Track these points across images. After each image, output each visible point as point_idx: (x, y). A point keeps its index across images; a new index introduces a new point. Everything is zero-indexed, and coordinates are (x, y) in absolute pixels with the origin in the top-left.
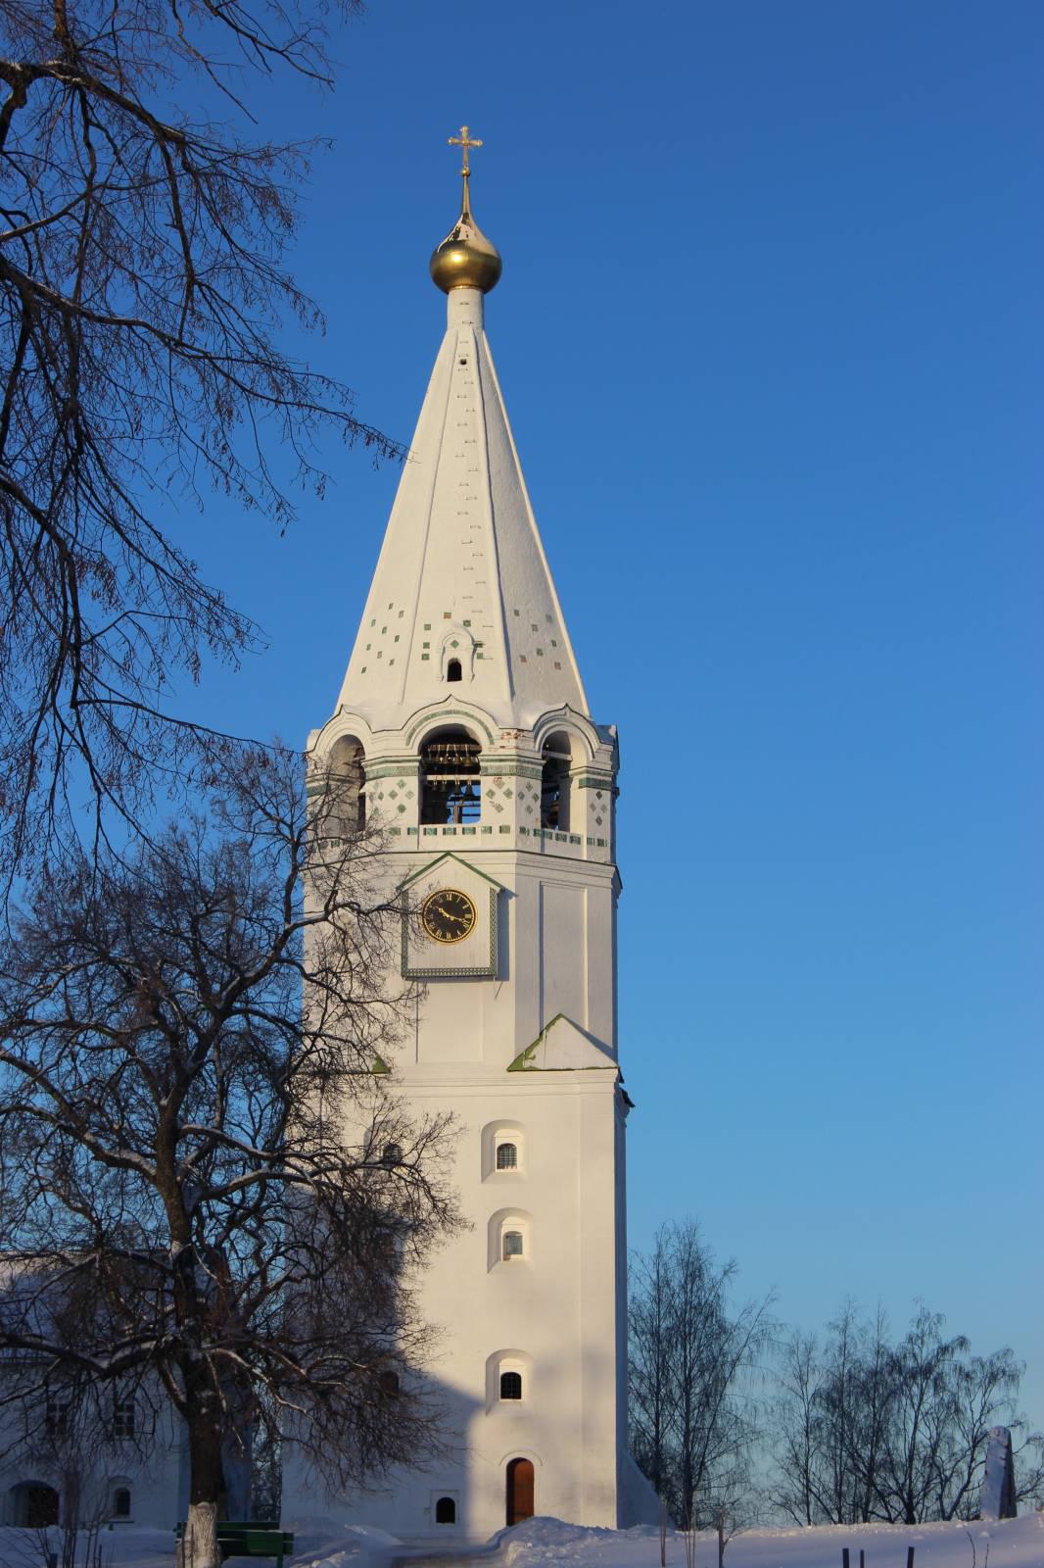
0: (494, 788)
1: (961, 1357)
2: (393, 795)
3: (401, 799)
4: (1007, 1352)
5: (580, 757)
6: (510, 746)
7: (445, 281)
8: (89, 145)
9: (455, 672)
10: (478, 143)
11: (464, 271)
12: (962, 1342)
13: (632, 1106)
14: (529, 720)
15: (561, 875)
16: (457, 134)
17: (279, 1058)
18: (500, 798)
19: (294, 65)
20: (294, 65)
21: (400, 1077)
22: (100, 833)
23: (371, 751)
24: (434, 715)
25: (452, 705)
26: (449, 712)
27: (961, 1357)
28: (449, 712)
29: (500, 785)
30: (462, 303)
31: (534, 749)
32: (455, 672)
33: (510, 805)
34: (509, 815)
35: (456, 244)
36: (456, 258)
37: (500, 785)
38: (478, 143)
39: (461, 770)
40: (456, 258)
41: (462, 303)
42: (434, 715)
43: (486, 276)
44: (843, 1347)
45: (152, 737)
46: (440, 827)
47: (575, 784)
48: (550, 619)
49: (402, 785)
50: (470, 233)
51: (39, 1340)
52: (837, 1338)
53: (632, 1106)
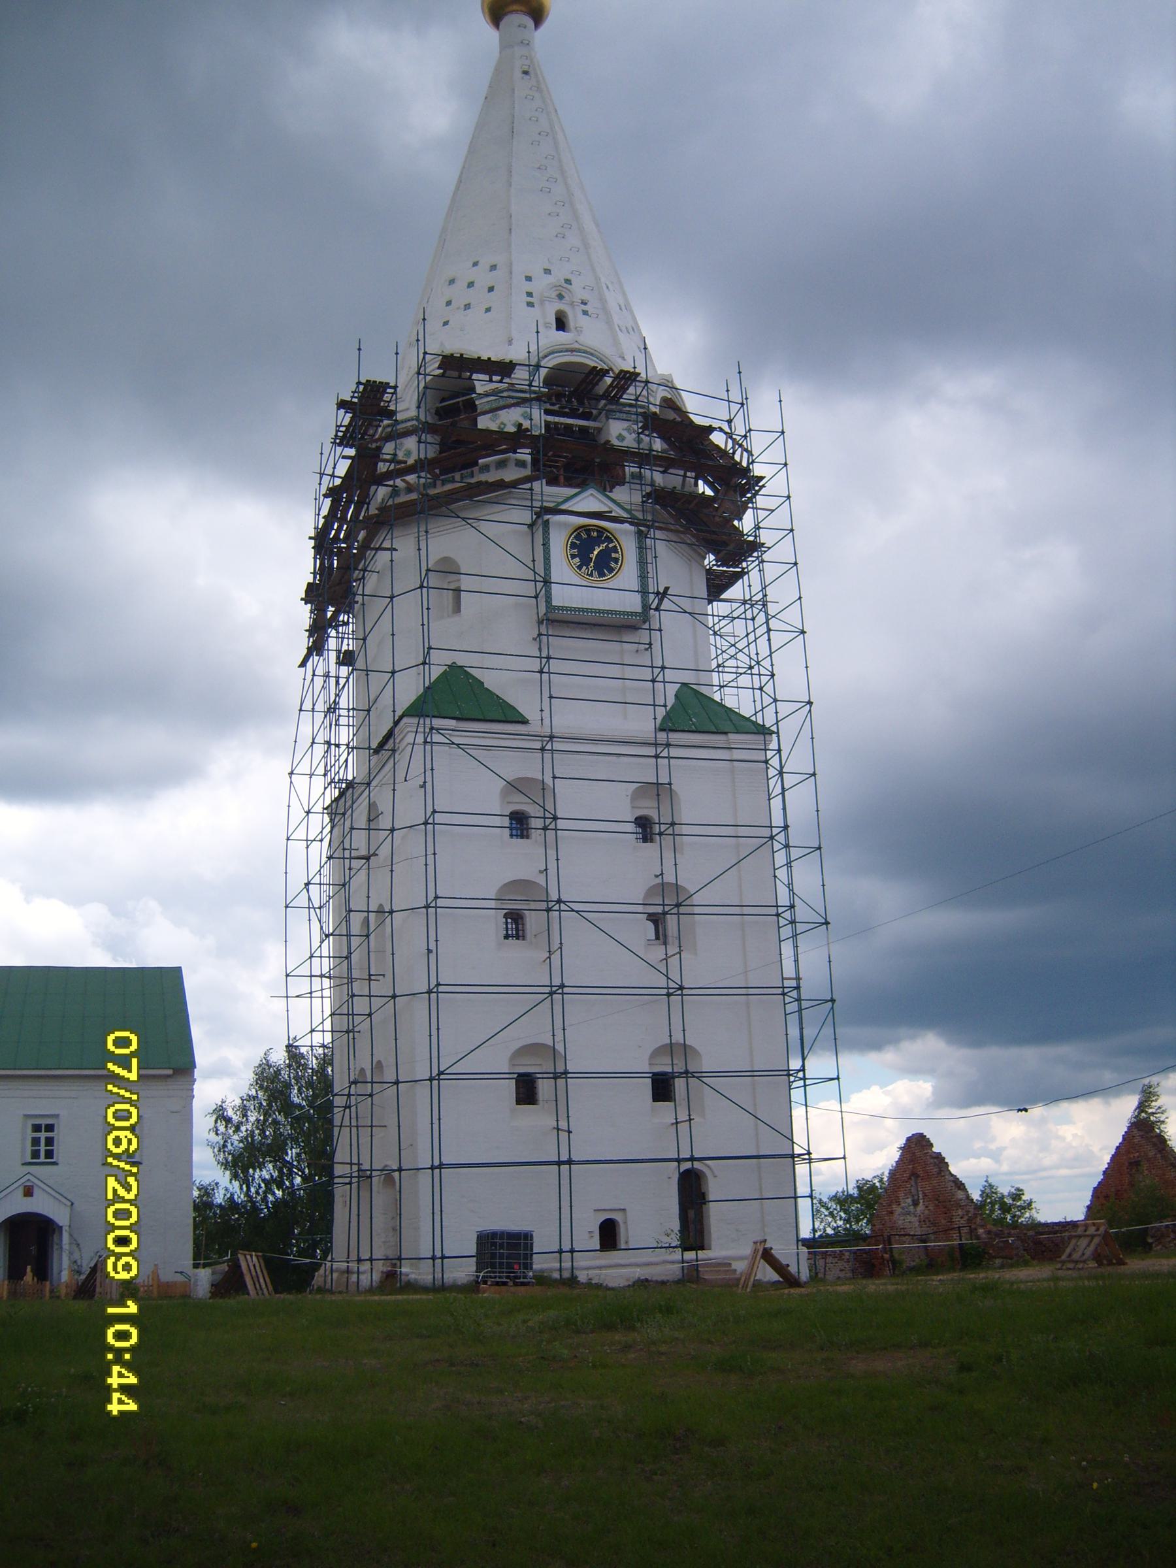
32: (561, 324)
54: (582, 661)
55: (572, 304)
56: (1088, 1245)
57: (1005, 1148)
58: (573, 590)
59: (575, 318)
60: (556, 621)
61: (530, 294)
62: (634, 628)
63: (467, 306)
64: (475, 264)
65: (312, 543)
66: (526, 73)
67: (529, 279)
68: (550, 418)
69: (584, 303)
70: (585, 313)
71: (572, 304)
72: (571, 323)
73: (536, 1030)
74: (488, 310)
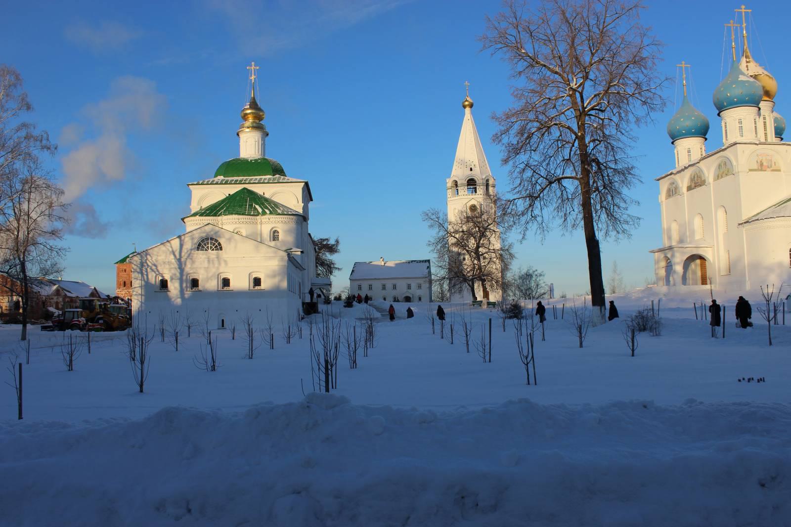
1: (536, 273)
3: (465, 190)
4: (543, 272)
5: (491, 182)
6: (481, 182)
7: (465, 107)
8: (559, 51)
9: (471, 170)
10: (469, 84)
11: (468, 105)
12: (536, 270)
14: (484, 177)
16: (465, 82)
18: (480, 189)
21: (64, 267)
23: (459, 183)
25: (472, 175)
27: (536, 273)
30: (468, 110)
31: (485, 181)
32: (471, 170)
33: (482, 190)
34: (481, 192)
35: (467, 101)
36: (467, 103)
38: (469, 84)
40: (467, 103)
41: (468, 110)
43: (471, 106)
44: (520, 272)
47: (490, 187)
48: (485, 160)
50: (468, 99)
51: (143, 287)
52: (519, 271)
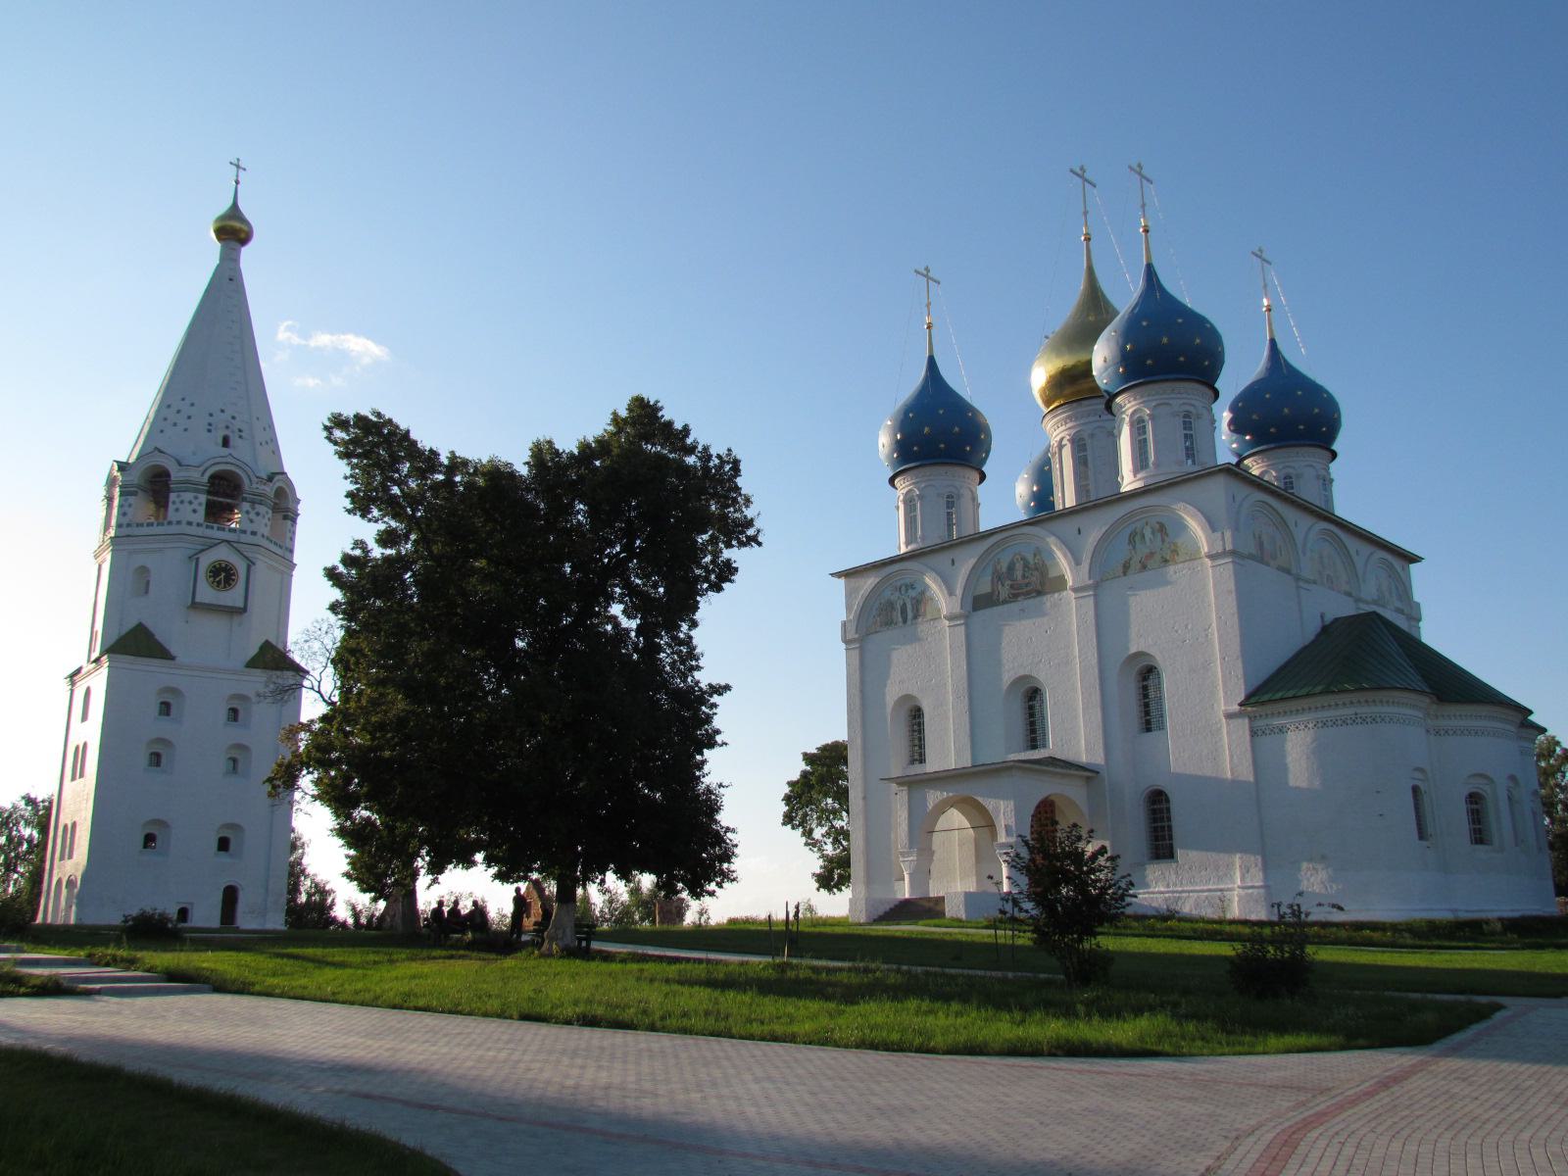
0: (250, 509)
2: (190, 503)
9: (226, 442)
13: (1413, 559)
15: (146, 546)
17: (169, 920)
19: (1142, 187)
20: (1142, 187)
22: (235, 545)
24: (218, 463)
25: (229, 460)
26: (227, 463)
28: (227, 463)
29: (253, 509)
32: (226, 442)
37: (253, 509)
39: (227, 496)
42: (218, 463)
45: (583, 1067)
46: (215, 526)
49: (196, 498)
53: (1413, 559)
54: (213, 627)
55: (233, 432)
56: (990, 1064)
57: (455, 867)
58: (207, 593)
59: (234, 440)
60: (195, 606)
61: (210, 425)
62: (241, 613)
63: (175, 424)
64: (183, 399)
65: (678, 426)
66: (231, 280)
67: (211, 415)
68: (210, 497)
69: (240, 431)
70: (240, 437)
71: (233, 432)
72: (231, 443)
73: (472, 899)
74: (186, 430)
